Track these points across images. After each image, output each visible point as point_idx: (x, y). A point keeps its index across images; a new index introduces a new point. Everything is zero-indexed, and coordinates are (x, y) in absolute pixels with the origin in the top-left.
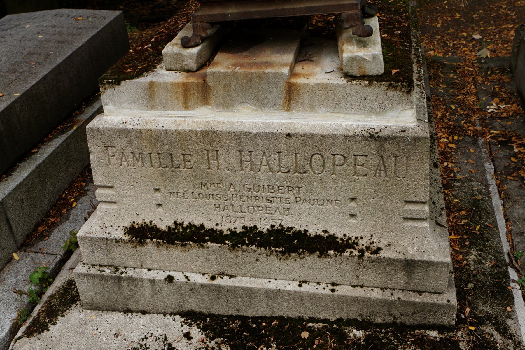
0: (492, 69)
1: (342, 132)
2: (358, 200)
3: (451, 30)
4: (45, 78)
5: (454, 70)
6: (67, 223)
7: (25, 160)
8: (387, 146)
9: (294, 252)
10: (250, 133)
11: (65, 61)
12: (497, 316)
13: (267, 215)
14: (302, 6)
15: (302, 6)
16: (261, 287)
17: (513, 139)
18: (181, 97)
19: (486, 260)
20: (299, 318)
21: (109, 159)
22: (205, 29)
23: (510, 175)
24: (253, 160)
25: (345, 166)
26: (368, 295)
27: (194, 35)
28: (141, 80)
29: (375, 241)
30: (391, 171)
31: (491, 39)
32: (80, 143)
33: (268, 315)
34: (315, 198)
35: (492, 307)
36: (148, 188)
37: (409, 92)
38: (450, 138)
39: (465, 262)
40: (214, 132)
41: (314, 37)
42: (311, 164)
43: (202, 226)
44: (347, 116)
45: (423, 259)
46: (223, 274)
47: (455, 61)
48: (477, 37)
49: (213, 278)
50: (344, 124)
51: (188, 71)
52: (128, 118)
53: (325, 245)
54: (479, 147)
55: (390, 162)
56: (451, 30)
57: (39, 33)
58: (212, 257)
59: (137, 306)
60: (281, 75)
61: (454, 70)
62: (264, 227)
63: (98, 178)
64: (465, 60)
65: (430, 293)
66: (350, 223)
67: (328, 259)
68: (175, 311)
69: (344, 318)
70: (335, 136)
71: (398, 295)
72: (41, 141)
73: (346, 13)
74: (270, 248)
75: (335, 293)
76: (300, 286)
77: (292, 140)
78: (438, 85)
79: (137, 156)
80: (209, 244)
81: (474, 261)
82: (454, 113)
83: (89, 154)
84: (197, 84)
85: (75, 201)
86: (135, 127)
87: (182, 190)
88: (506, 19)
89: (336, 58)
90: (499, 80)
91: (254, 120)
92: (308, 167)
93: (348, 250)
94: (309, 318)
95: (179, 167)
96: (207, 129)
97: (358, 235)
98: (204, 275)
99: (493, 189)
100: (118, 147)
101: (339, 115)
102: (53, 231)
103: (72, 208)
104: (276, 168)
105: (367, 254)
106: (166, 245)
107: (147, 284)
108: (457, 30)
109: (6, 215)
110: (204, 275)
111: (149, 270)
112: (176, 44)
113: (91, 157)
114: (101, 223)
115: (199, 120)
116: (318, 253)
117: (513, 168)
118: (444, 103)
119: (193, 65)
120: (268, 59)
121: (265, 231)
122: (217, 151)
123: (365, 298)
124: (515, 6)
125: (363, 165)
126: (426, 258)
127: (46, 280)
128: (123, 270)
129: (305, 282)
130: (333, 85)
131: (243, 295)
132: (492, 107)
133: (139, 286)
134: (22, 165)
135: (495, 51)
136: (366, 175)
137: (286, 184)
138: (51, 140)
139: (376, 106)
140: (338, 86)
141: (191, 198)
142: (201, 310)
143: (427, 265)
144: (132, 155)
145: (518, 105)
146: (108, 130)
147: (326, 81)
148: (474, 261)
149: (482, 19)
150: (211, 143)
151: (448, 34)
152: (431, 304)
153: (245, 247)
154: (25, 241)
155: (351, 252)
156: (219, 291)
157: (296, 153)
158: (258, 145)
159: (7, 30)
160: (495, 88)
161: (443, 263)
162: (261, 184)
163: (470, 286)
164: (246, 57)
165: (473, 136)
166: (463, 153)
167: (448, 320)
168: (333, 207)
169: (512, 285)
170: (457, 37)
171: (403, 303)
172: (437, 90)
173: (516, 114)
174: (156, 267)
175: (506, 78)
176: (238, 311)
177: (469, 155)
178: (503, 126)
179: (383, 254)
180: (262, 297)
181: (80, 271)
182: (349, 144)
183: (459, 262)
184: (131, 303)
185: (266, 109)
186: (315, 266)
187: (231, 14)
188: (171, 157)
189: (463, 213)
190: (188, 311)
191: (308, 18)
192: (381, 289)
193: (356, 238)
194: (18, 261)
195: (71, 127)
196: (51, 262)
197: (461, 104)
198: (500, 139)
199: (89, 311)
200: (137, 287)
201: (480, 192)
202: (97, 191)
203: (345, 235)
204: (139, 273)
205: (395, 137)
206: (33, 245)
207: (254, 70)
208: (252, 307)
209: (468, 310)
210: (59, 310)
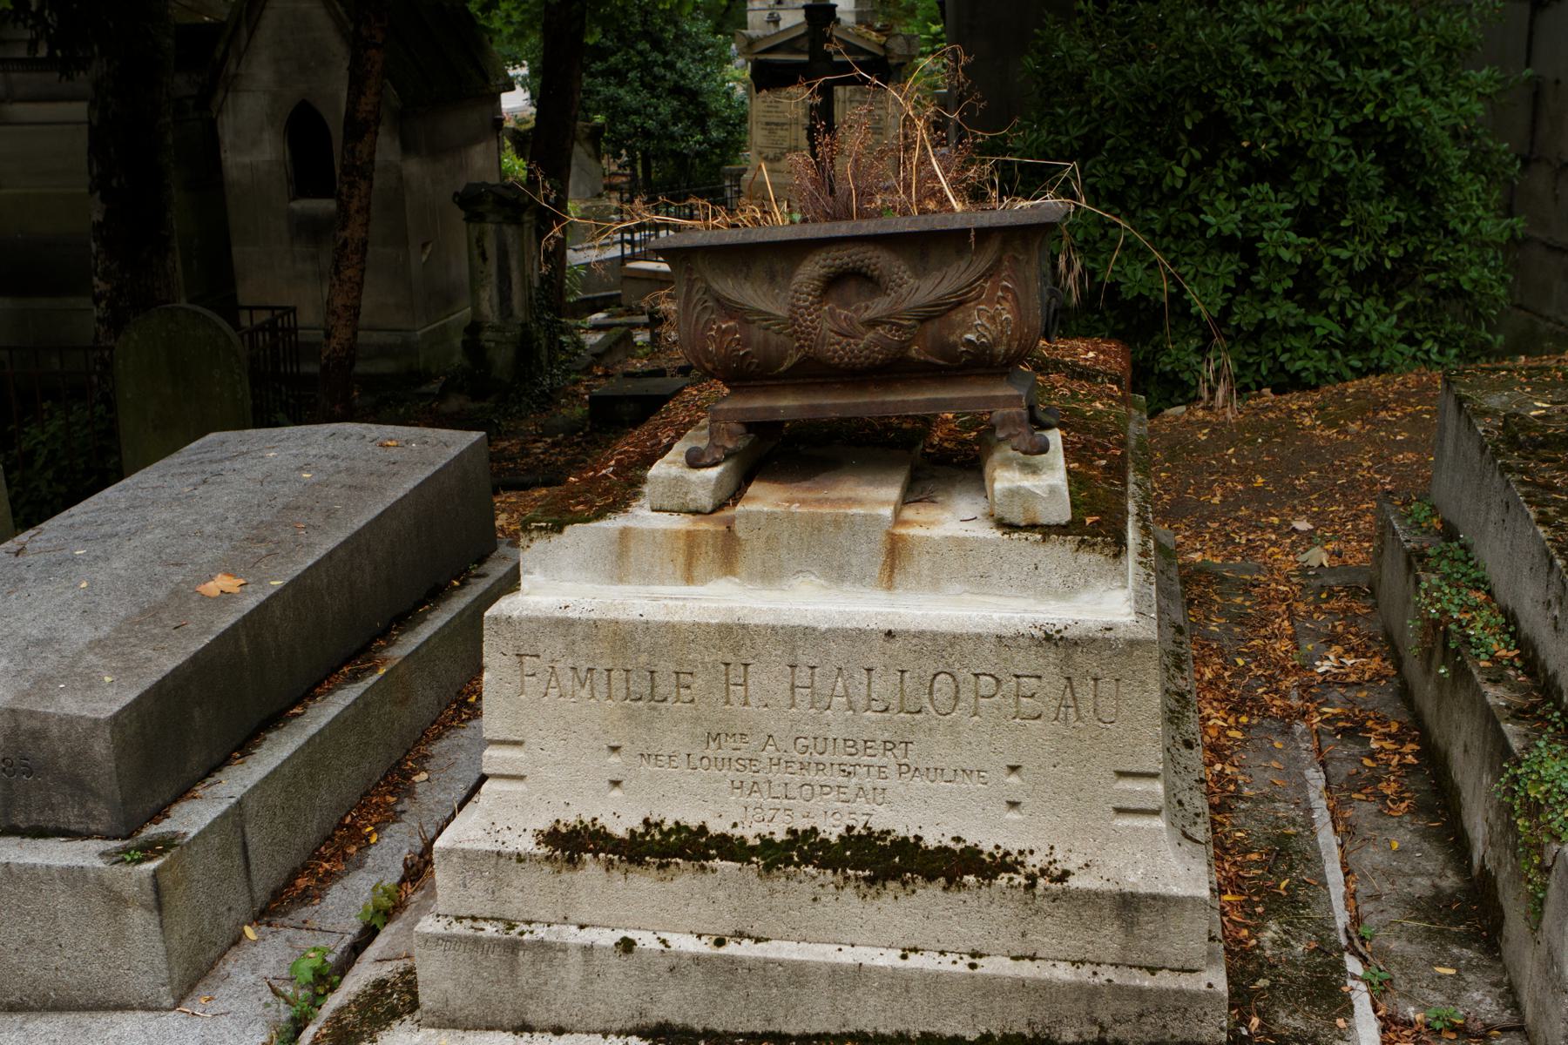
0: (1331, 588)
1: (993, 629)
2: (1023, 770)
3: (1243, 512)
4: (330, 555)
5: (1247, 588)
6: (361, 874)
7: (277, 728)
8: (1078, 657)
9: (893, 879)
10: (814, 629)
11: (369, 524)
12: (1315, 1035)
13: (839, 804)
14: (919, 397)
15: (919, 397)
16: (822, 959)
17: (1369, 724)
18: (681, 559)
19: (1299, 941)
20: (900, 1034)
21: (523, 682)
22: (731, 435)
23: (1359, 791)
24: (817, 684)
25: (997, 698)
26: (1046, 975)
27: (713, 445)
28: (603, 524)
29: (1058, 857)
30: (1087, 706)
31: (1335, 532)
32: (388, 708)
33: (834, 1030)
34: (938, 765)
35: (1307, 1019)
36: (595, 744)
37: (1116, 556)
38: (1231, 720)
39: (1254, 942)
40: (744, 627)
41: (940, 463)
42: (931, 693)
43: (703, 829)
44: (1002, 601)
45: (1154, 891)
46: (740, 935)
47: (1248, 571)
48: (1302, 525)
49: (720, 942)
50: (996, 616)
51: (696, 512)
52: (569, 600)
53: (957, 866)
54: (1293, 740)
55: (1085, 690)
56: (1243, 512)
57: (301, 469)
58: (721, 894)
59: (546, 1016)
60: (877, 519)
61: (1247, 588)
62: (832, 831)
63: (493, 721)
64: (1271, 571)
65: (1172, 970)
66: (1007, 821)
67: (964, 895)
68: (630, 1025)
69: (995, 1032)
70: (979, 636)
71: (1107, 973)
72: (309, 692)
73: (999, 413)
74: (844, 871)
75: (977, 971)
76: (904, 957)
77: (897, 645)
78: (1207, 618)
79: (582, 675)
80: (717, 863)
81: (1274, 942)
82: (1240, 673)
83: (480, 670)
84: (715, 535)
85: (377, 830)
86: (585, 616)
87: (667, 751)
88: (1370, 490)
89: (981, 500)
90: (1344, 612)
91: (822, 607)
92: (925, 700)
93: (1006, 876)
94: (922, 1033)
95: (665, 700)
96: (729, 621)
97: (1025, 846)
98: (699, 936)
99: (1321, 816)
100: (546, 656)
101: (987, 599)
102: (329, 888)
103: (369, 846)
104: (863, 702)
105: (1042, 882)
106: (625, 865)
107: (576, 958)
108: (1257, 512)
109: (244, 835)
110: (699, 936)
111: (582, 927)
112: (674, 462)
113: (486, 676)
114: (486, 823)
115: (714, 605)
116: (942, 880)
117: (1367, 779)
118: (1220, 652)
119: (706, 502)
120: (852, 494)
121: (834, 839)
122: (746, 665)
123: (1038, 980)
124: (1391, 464)
125: (1032, 696)
126: (1160, 889)
127: (325, 980)
128: (525, 927)
129: (916, 950)
130: (976, 539)
131: (783, 980)
132: (1326, 663)
133: (556, 962)
134: (273, 735)
135: (1339, 555)
136: (1039, 717)
137: (880, 738)
138: (330, 692)
139: (1056, 581)
140: (985, 542)
141: (684, 766)
142: (688, 1021)
143: (1163, 903)
144: (571, 674)
145: (1384, 660)
146: (530, 620)
147: (962, 534)
148: (1274, 942)
149: (1314, 489)
150: (735, 650)
151: (1236, 519)
152: (1176, 992)
153: (792, 868)
154: (268, 904)
155: (1011, 879)
156: (731, 972)
157: (903, 672)
158: (828, 654)
159: (221, 461)
160: (1334, 627)
161: (1193, 898)
162: (831, 736)
163: (1262, 983)
164: (809, 489)
165: (1283, 718)
166: (1259, 750)
167: (1212, 1029)
168: (973, 784)
169: (1351, 983)
170: (1257, 527)
171: (1119, 991)
172: (1205, 626)
173: (1379, 676)
174: (598, 920)
175: (1360, 607)
176: (769, 1021)
177: (1272, 754)
178: (1349, 701)
179: (1074, 883)
180: (823, 983)
181: (430, 930)
182: (1005, 653)
183: (1241, 942)
184: (532, 1008)
185: (847, 586)
186: (937, 911)
187: (785, 408)
188: (652, 679)
189: (1254, 857)
190: (659, 1024)
191: (927, 422)
192: (1073, 963)
193: (1021, 853)
194: (255, 943)
195: (374, 669)
196: (336, 947)
197: (1255, 655)
198: (1340, 724)
199: (433, 1031)
200: (551, 966)
201: (1293, 822)
202: (487, 753)
203: (997, 847)
204: (559, 934)
205: (1094, 640)
206: (286, 914)
207: (826, 510)
208: (800, 1010)
209: (1255, 1021)
210: (362, 1032)
